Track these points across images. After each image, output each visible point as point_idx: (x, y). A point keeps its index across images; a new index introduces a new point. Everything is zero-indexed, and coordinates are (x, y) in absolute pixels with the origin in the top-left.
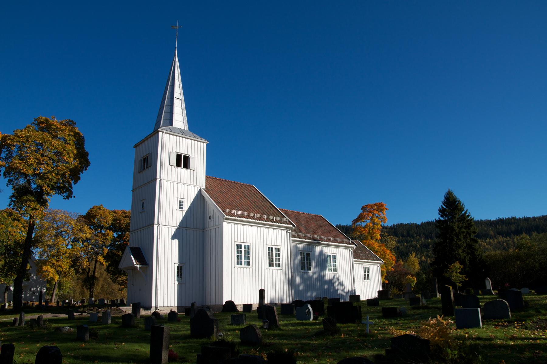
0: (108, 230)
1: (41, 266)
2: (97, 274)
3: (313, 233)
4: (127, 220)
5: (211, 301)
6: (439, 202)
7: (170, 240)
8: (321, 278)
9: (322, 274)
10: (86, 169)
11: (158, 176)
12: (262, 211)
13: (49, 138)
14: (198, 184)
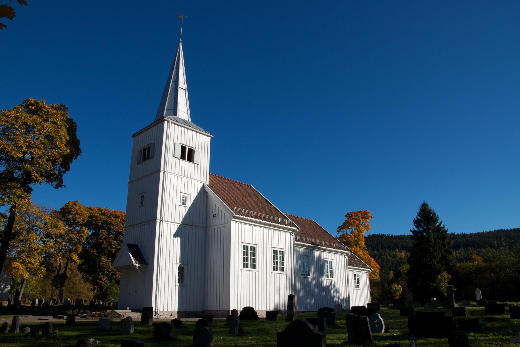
0: (84, 227)
1: (10, 262)
2: (69, 273)
3: (311, 237)
4: (104, 218)
5: (214, 306)
6: (414, 213)
8: (319, 284)
10: (76, 158)
11: (162, 168)
12: (266, 213)
13: (39, 120)
14: (202, 180)
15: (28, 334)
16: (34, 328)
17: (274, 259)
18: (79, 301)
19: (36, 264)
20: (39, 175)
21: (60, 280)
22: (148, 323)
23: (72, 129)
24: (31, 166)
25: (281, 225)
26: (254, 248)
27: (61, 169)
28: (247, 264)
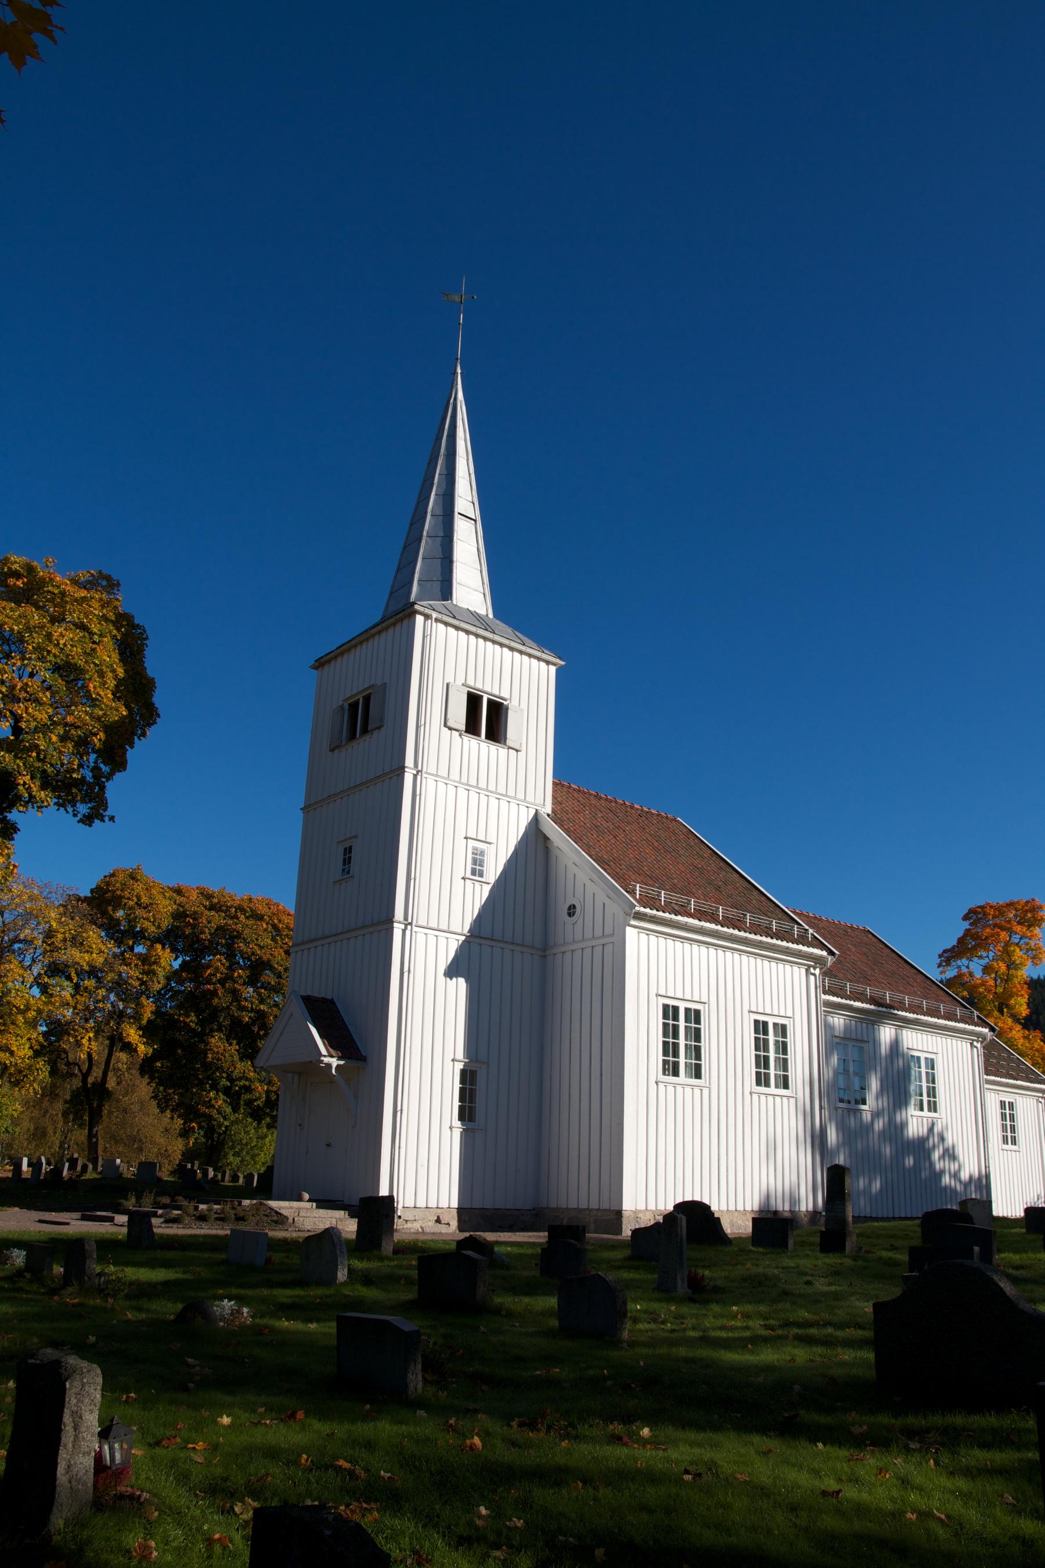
0: (159, 946)
3: (867, 981)
4: (218, 919)
5: (572, 1194)
7: (441, 978)
8: (895, 1130)
9: (898, 1118)
10: (144, 734)
11: (409, 761)
12: (731, 903)
14: (530, 798)
15: (19, 1273)
16: (40, 1251)
17: (757, 1048)
18: (147, 1168)
19: (21, 1054)
20: (38, 783)
21: (90, 1101)
22: (379, 1246)
23: (131, 645)
24: (16, 757)
25: (779, 942)
26: (697, 1013)
27: (102, 766)
28: (676, 1065)
